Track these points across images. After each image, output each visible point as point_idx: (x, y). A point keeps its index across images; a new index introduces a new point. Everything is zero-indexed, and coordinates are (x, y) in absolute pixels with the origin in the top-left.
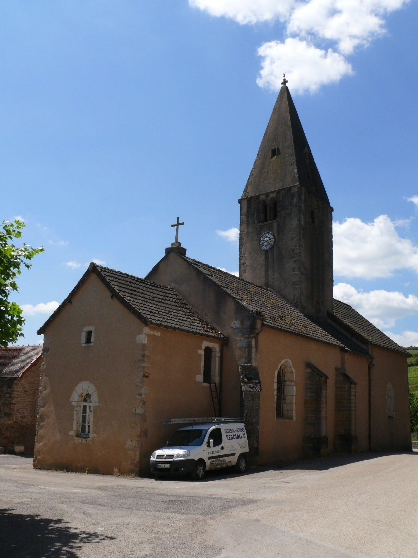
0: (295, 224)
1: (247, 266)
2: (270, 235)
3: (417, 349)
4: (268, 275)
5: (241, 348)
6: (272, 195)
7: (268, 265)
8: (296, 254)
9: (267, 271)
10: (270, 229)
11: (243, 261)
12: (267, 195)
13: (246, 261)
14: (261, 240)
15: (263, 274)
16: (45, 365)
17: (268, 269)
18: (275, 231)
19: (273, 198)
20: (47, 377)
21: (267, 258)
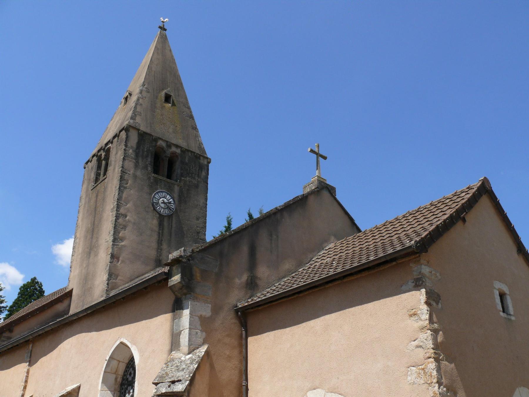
0: (202, 202)
1: (129, 221)
2: (157, 195)
3: (240, 392)
4: (161, 249)
5: (420, 368)
6: (174, 149)
7: (162, 235)
8: (201, 239)
9: (160, 242)
10: (170, 191)
11: (122, 211)
12: (169, 145)
13: (129, 215)
14: (168, 196)
15: (154, 245)
16: (441, 332)
17: (162, 240)
18: (176, 195)
19: (174, 153)
20: (450, 362)
21: (161, 224)
